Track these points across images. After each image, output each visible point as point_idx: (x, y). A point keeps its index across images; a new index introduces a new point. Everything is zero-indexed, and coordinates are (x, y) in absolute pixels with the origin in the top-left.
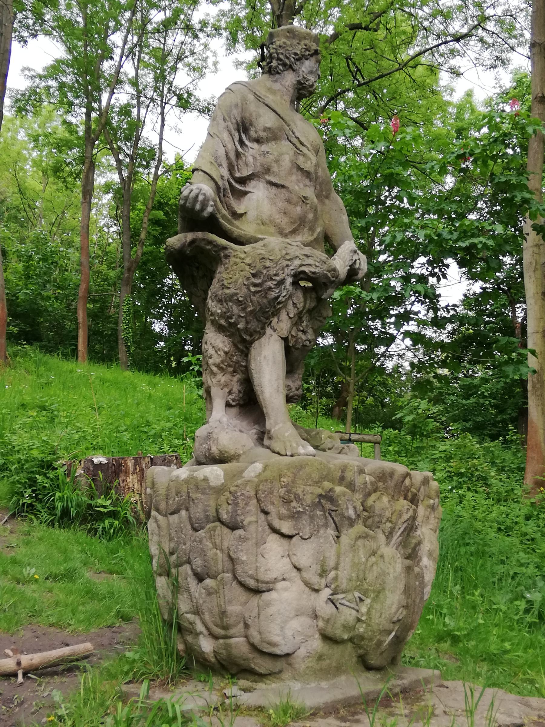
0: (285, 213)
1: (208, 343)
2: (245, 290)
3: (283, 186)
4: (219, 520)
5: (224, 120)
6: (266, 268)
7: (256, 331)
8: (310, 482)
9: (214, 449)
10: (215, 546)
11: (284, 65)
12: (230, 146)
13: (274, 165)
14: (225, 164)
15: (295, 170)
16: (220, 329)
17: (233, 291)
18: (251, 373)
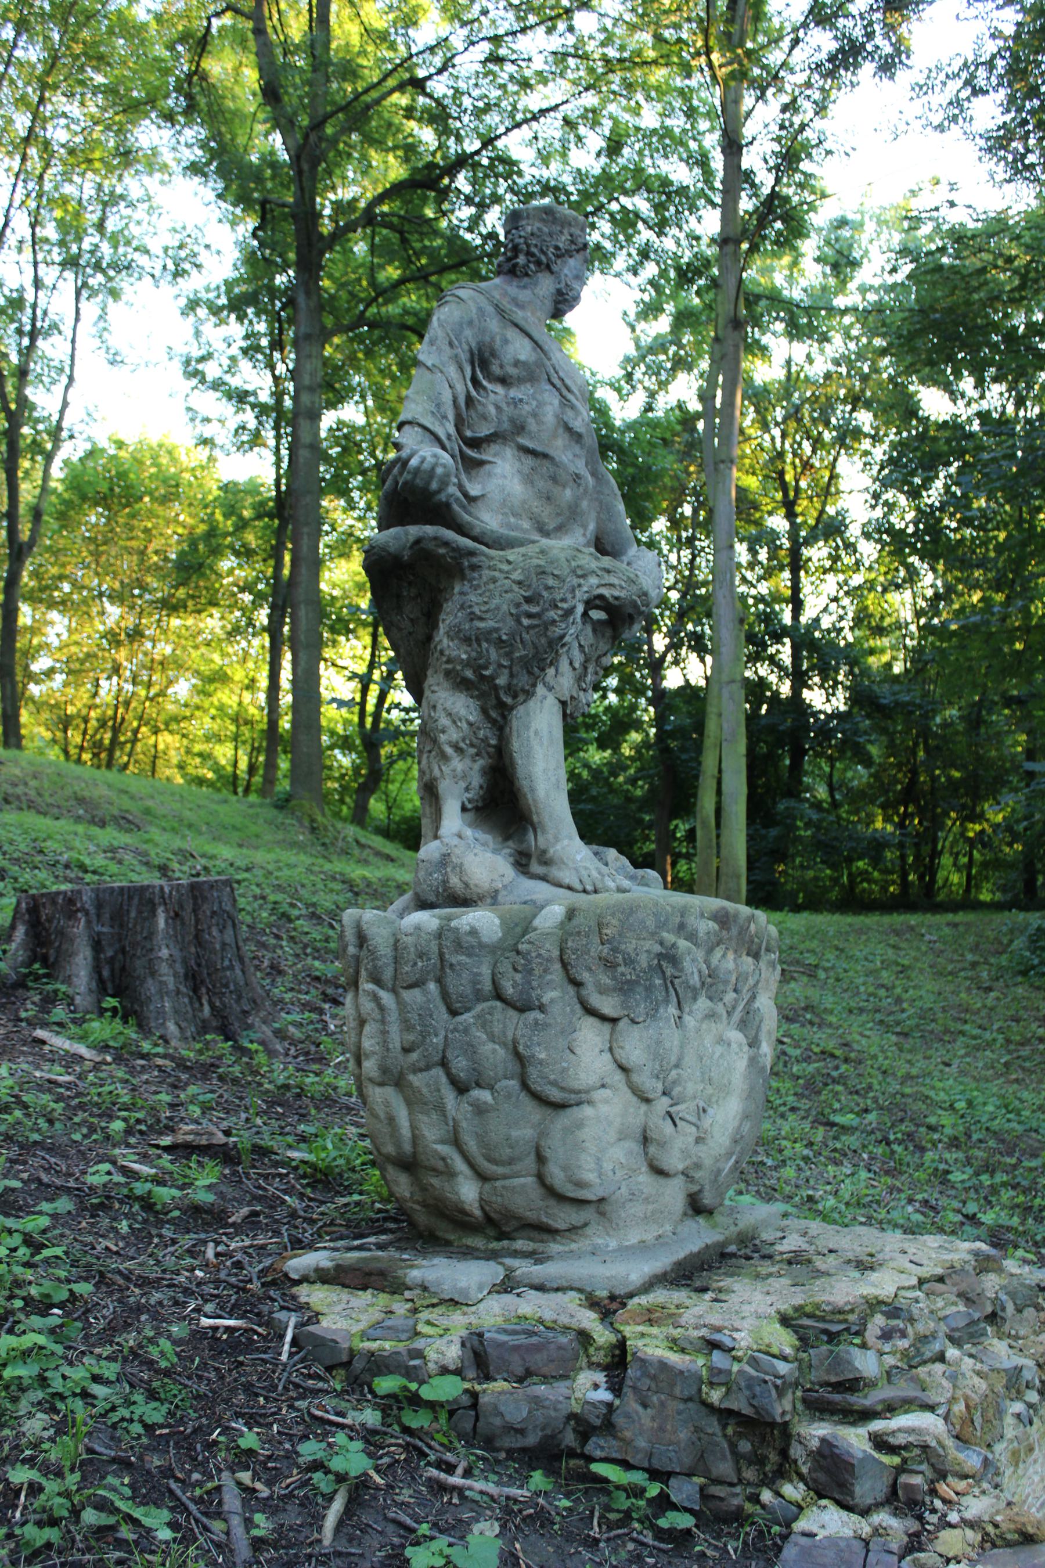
0: (548, 498)
1: (439, 707)
2: (511, 622)
3: (545, 456)
4: (499, 996)
5: (451, 344)
6: (548, 588)
7: (523, 691)
8: (645, 934)
9: (454, 881)
10: (492, 1038)
11: (538, 263)
12: (460, 388)
13: (531, 420)
14: (451, 416)
15: (561, 430)
16: (462, 685)
17: (491, 624)
18: (511, 757)
